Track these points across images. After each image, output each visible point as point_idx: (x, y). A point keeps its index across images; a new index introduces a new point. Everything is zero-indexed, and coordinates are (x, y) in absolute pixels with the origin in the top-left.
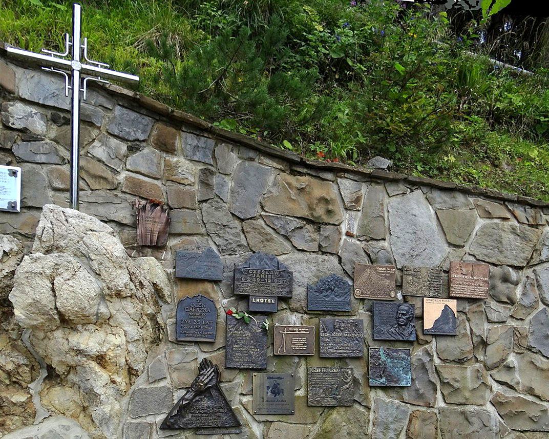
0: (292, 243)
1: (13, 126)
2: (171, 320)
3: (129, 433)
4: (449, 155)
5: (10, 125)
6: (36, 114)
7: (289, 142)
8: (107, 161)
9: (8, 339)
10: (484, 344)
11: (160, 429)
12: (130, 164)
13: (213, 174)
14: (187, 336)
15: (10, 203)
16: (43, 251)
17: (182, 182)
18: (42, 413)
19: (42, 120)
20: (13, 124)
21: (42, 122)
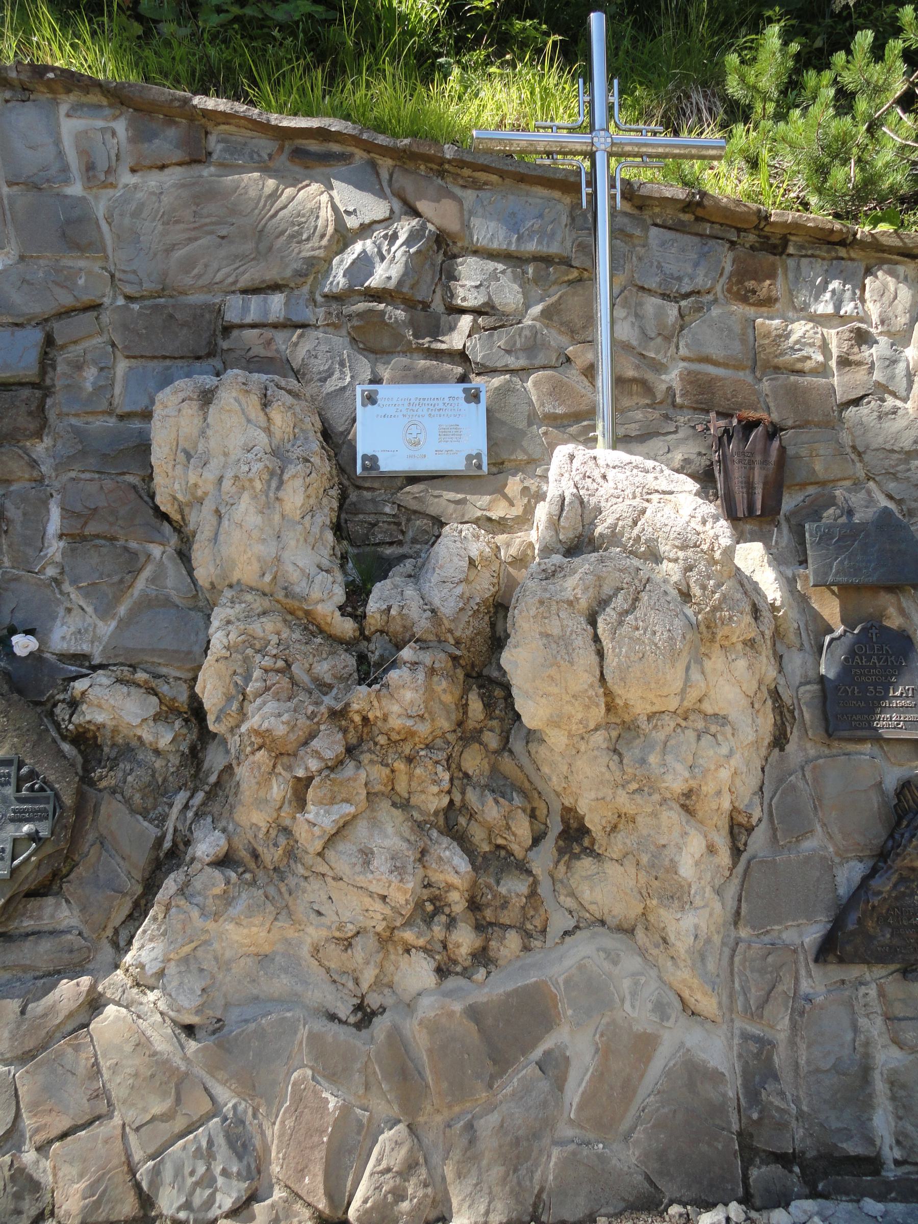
0: (219, 524)
1: (465, 304)
2: (808, 687)
3: (748, 973)
4: (705, 547)
5: (459, 302)
6: (503, 272)
7: (370, 1022)
8: (640, 345)
9: (292, 881)
10: (316, 357)
11: (816, 960)
12: (687, 345)
13: (866, 342)
14: (856, 728)
15: (469, 458)
16: (562, 550)
17: (799, 366)
18: (560, 922)
19: (515, 282)
20: (464, 299)
21: (516, 287)
